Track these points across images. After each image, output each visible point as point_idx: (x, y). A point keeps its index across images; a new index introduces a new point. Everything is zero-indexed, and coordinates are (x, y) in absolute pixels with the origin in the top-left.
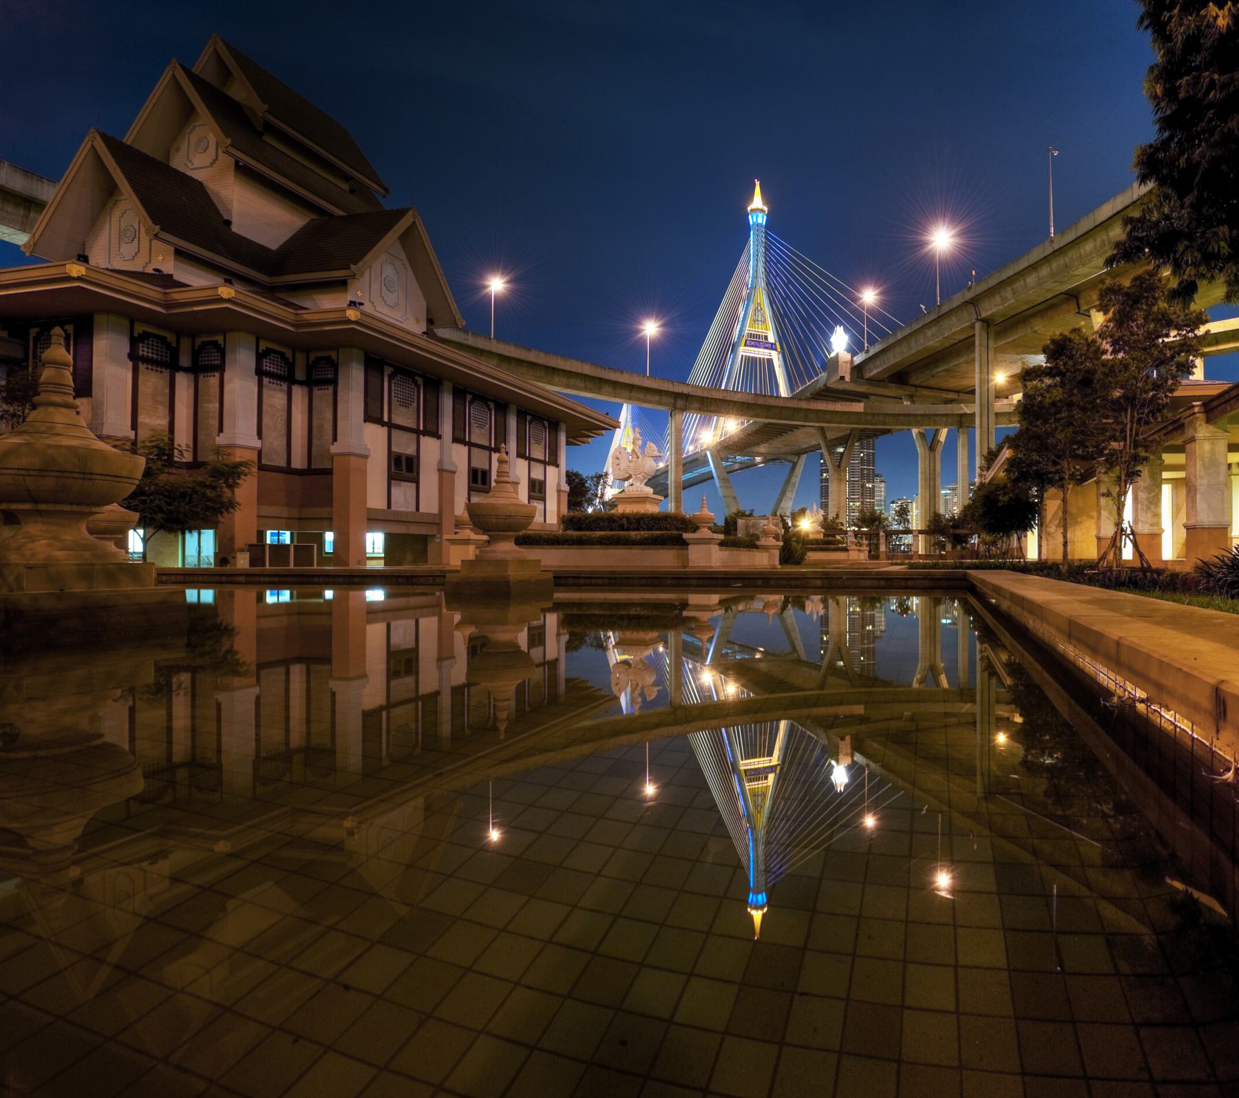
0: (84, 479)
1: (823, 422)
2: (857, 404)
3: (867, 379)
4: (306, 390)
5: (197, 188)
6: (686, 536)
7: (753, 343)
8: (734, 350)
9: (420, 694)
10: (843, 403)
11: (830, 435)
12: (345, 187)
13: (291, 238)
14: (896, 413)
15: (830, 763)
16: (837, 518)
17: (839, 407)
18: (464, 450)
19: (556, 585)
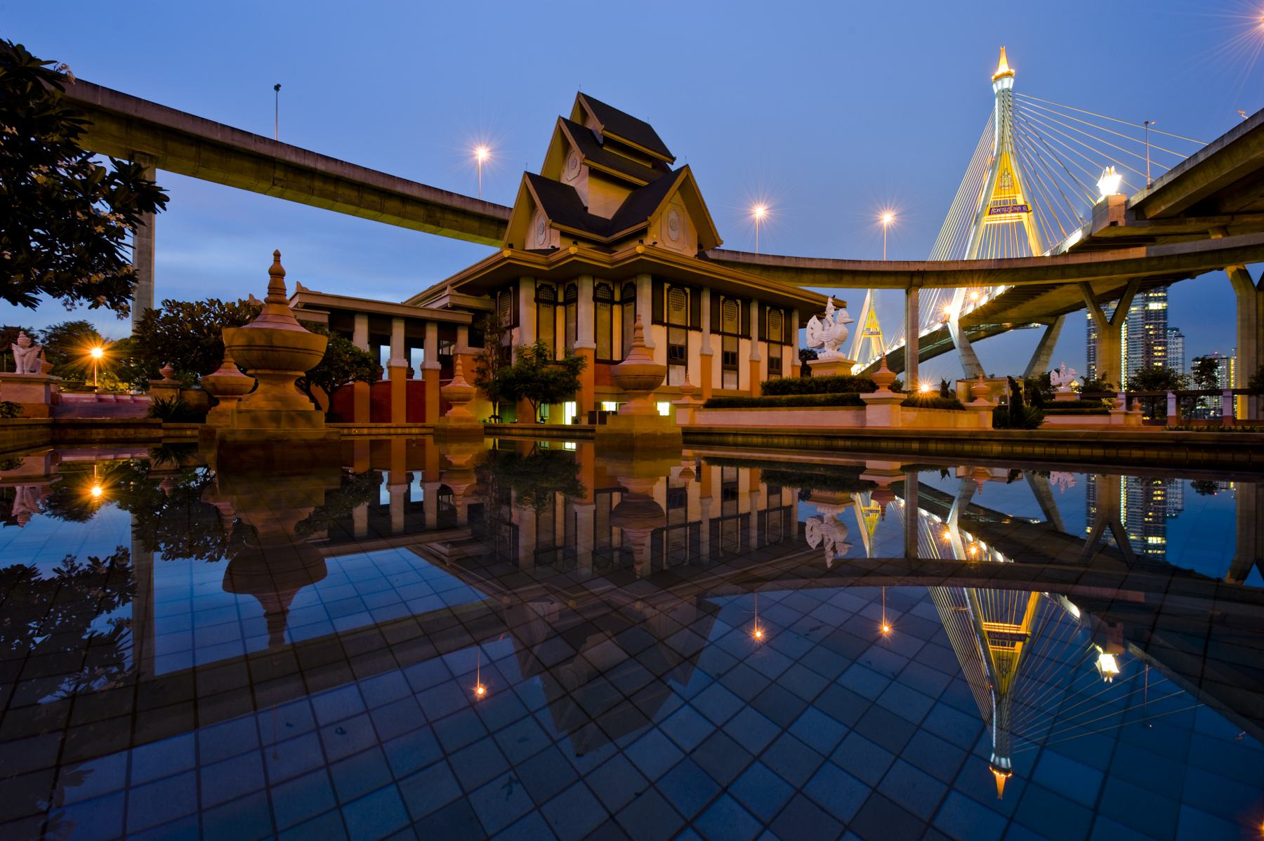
0: (272, 351)
1: (1085, 276)
2: (1138, 249)
3: (1151, 219)
4: (620, 306)
5: (571, 190)
6: (863, 396)
7: (999, 210)
8: (977, 221)
9: (739, 513)
10: (1116, 251)
11: (1098, 290)
12: (649, 166)
13: (620, 209)
14: (1198, 250)
15: (1094, 647)
16: (1103, 379)
17: (1110, 256)
18: (663, 330)
19: (685, 442)
